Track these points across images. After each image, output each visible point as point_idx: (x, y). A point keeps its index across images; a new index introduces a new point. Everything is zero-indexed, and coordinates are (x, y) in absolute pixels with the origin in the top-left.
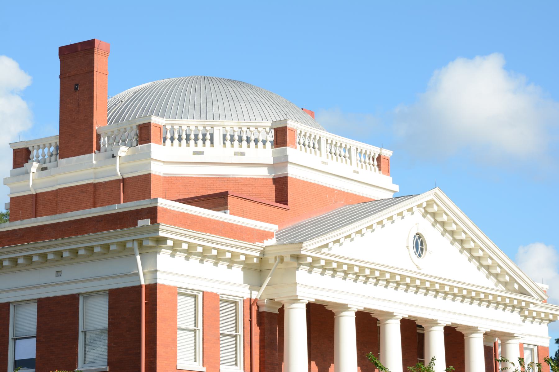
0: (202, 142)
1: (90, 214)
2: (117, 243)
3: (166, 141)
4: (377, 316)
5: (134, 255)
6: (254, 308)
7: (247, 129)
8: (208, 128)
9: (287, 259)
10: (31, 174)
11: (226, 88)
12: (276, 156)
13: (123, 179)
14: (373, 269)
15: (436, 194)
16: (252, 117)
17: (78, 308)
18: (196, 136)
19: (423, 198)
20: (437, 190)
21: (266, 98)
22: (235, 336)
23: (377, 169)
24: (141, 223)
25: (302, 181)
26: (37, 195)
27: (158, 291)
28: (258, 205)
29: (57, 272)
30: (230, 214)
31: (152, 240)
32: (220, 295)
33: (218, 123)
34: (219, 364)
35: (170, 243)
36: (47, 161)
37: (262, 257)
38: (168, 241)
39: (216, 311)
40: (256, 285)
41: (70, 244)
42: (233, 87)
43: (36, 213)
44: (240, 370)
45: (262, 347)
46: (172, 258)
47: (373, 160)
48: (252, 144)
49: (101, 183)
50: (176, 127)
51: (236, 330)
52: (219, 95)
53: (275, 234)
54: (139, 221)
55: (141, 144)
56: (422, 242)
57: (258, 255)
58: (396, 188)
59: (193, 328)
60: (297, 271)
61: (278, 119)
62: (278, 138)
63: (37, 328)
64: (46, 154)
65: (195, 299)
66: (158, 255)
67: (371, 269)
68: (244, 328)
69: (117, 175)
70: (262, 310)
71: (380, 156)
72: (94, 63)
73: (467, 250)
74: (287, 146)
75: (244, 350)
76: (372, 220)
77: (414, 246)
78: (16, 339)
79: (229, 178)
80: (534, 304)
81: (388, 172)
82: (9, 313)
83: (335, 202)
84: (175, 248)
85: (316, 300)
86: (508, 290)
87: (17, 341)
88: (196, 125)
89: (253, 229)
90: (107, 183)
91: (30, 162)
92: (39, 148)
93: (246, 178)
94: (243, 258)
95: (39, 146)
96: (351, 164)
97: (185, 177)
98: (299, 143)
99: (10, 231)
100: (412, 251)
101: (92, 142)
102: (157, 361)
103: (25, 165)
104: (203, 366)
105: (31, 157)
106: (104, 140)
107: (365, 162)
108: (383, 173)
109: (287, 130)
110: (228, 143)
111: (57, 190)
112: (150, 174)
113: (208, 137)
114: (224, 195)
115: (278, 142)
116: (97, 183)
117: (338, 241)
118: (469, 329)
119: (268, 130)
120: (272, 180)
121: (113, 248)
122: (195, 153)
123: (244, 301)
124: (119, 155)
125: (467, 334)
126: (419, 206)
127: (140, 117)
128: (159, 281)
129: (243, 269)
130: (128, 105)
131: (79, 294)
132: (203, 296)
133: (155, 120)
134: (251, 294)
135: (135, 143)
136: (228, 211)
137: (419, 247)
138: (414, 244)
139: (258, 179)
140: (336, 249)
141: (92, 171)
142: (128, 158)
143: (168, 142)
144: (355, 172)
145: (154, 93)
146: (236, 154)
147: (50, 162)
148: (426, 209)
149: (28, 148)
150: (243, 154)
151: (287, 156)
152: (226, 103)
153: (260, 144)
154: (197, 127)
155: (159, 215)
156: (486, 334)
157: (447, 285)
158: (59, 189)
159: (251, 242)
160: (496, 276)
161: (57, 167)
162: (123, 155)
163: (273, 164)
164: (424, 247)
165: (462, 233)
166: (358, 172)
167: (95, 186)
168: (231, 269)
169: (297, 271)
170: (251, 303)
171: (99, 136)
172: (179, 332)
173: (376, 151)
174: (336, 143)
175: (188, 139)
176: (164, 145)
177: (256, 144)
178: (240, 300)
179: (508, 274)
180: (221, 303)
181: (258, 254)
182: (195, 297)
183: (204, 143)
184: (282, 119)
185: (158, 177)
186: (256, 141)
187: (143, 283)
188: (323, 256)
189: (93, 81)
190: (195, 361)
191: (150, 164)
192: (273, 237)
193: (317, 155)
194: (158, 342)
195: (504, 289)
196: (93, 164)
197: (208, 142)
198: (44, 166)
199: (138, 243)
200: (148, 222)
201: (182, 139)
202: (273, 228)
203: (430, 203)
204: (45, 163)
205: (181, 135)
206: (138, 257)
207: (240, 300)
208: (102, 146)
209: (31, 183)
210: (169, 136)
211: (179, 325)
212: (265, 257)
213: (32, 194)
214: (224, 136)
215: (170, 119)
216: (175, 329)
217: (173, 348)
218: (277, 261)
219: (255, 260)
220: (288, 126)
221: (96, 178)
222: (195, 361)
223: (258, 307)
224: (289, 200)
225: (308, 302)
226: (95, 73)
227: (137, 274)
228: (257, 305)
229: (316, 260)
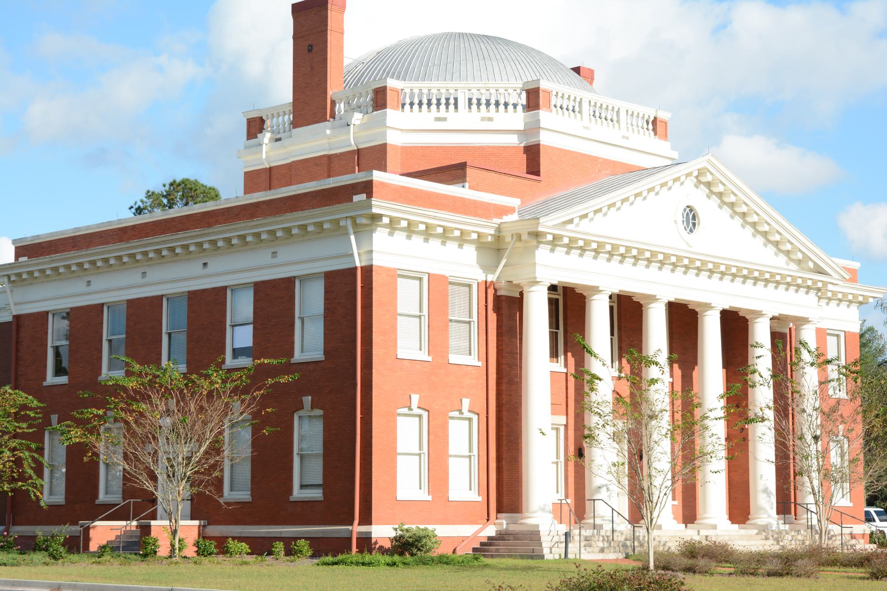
0: (445, 107)
2: (330, 221)
3: (405, 107)
4: (638, 299)
5: (347, 234)
6: (491, 292)
7: (504, 92)
8: (452, 91)
9: (525, 237)
10: (264, 145)
11: (477, 45)
13: (358, 149)
14: (629, 247)
15: (709, 161)
18: (439, 100)
19: (694, 166)
20: (709, 157)
21: (524, 55)
22: (469, 323)
23: (652, 133)
24: (356, 198)
25: (558, 149)
27: (374, 273)
28: (503, 176)
30: (470, 188)
31: (366, 217)
32: (450, 278)
33: (463, 85)
34: (448, 353)
35: (386, 220)
36: (282, 131)
37: (497, 234)
40: (488, 268)
41: (282, 222)
42: (486, 44)
43: (270, 186)
44: (474, 359)
47: (648, 123)
48: (502, 107)
49: (336, 154)
51: (470, 315)
52: (468, 54)
55: (377, 111)
56: (694, 217)
57: (492, 232)
58: (675, 155)
59: (418, 313)
60: (536, 251)
61: (530, 79)
62: (530, 101)
64: (274, 124)
65: (420, 282)
66: (374, 234)
67: (626, 247)
70: (499, 293)
71: (655, 118)
72: (327, 21)
73: (749, 224)
74: (539, 109)
75: (478, 338)
76: (629, 191)
77: (683, 221)
78: (235, 326)
79: (475, 147)
81: (665, 137)
83: (599, 171)
84: (393, 224)
85: (559, 282)
86: (803, 269)
87: (236, 328)
88: (477, 87)
89: (489, 204)
91: (264, 131)
92: (279, 116)
93: (494, 147)
95: (284, 112)
96: (619, 129)
97: (425, 147)
98: (555, 106)
99: (226, 208)
100: (681, 227)
101: (326, 109)
102: (373, 350)
103: (259, 135)
104: (429, 355)
106: (341, 107)
107: (643, 128)
108: (660, 138)
109: (540, 91)
110: (474, 107)
111: (290, 163)
113: (452, 101)
114: (462, 166)
115: (530, 105)
116: (331, 155)
117: (585, 216)
118: (753, 313)
119: (518, 91)
120: (523, 148)
121: (326, 226)
123: (478, 283)
124: (353, 123)
125: (751, 318)
126: (688, 175)
127: (374, 80)
129: (477, 248)
130: (369, 67)
131: (295, 277)
132: (845, 336)
133: (391, 83)
134: (486, 276)
135: (370, 109)
136: (467, 184)
138: (683, 218)
139: (508, 147)
140: (585, 226)
142: (363, 127)
143: (407, 107)
144: (623, 137)
145: (397, 53)
146: (483, 119)
147: (284, 132)
149: (262, 117)
150: (490, 119)
151: (539, 120)
153: (510, 107)
154: (439, 90)
156: (773, 319)
157: (722, 264)
158: (293, 162)
159: (487, 218)
160: (787, 253)
161: (291, 137)
162: (358, 123)
163: (524, 130)
164: (697, 222)
165: (743, 205)
166: (627, 138)
167: (330, 158)
169: (536, 251)
170: (487, 285)
171: (333, 103)
172: (399, 318)
173: (651, 113)
174: (601, 104)
176: (403, 111)
177: (506, 108)
178: (474, 282)
179: (800, 250)
180: (450, 286)
182: (420, 279)
183: (447, 108)
184: (535, 78)
185: (395, 147)
186: (506, 105)
187: (358, 264)
188: (567, 233)
190: (421, 350)
191: (386, 132)
192: (515, 212)
193: (484, 122)
196: (327, 135)
197: (452, 107)
198: (278, 136)
199: (352, 221)
200: (363, 197)
203: (701, 172)
204: (279, 133)
205: (431, 100)
206: (352, 237)
207: (474, 282)
208: (337, 113)
209: (264, 157)
210: (408, 101)
211: (399, 311)
212: (501, 234)
213: (266, 168)
214: (470, 100)
215: (412, 82)
216: (394, 315)
217: (392, 336)
218: (514, 240)
219: (490, 239)
220: (541, 87)
221: (330, 149)
222: (421, 350)
223: (496, 290)
224: (541, 171)
225: (549, 285)
226: (329, 32)
227: (352, 255)
228: (494, 288)
229: (556, 238)
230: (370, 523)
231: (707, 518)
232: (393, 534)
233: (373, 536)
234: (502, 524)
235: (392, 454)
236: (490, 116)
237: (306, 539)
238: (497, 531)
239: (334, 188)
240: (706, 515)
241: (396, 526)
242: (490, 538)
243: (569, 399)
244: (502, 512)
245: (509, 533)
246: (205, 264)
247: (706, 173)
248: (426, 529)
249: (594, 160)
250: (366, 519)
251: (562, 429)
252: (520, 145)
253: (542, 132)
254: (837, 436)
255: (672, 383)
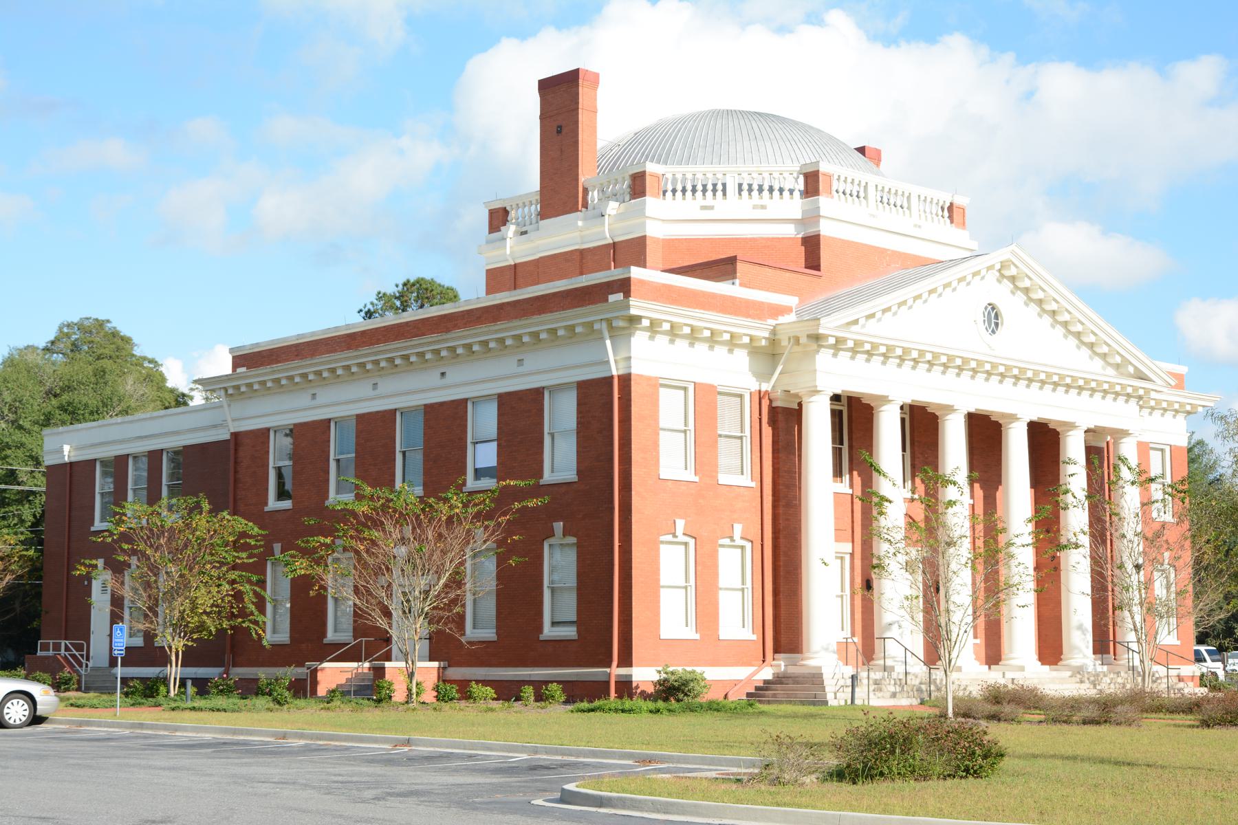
1: (553, 288)
2: (583, 324)
5: (602, 339)
6: (765, 403)
8: (720, 176)
9: (803, 340)
10: (508, 240)
11: (748, 123)
12: (807, 208)
15: (1013, 252)
16: (779, 160)
17: (543, 405)
18: (704, 186)
22: (741, 438)
24: (612, 298)
26: (515, 265)
28: (779, 272)
29: (519, 360)
30: (741, 285)
31: (623, 319)
34: (717, 472)
35: (646, 323)
37: (772, 337)
38: (643, 320)
39: (713, 407)
40: (763, 376)
45: (775, 451)
46: (651, 342)
47: (943, 209)
48: (776, 193)
49: (589, 248)
50: (679, 176)
53: (794, 310)
54: (610, 296)
56: (996, 316)
63: (498, 429)
68: (751, 427)
69: (606, 238)
70: (774, 404)
71: (951, 204)
74: (818, 195)
78: (477, 443)
79: (746, 239)
80: (1156, 391)
82: (466, 412)
84: (654, 327)
86: (1122, 374)
87: (478, 446)
90: (596, 249)
92: (525, 206)
94: (746, 340)
95: (531, 202)
96: (911, 216)
98: (837, 191)
101: (578, 197)
105: (509, 218)
106: (594, 196)
110: (745, 193)
112: (644, 237)
113: (720, 187)
114: (732, 261)
116: (584, 249)
117: (872, 316)
122: (703, 208)
123: (751, 393)
126: (990, 268)
127: (632, 164)
128: (634, 371)
129: (750, 354)
130: (625, 149)
133: (651, 168)
134: (760, 385)
135: (627, 198)
136: (737, 281)
137: (993, 321)
141: (577, 234)
142: (620, 217)
143: (669, 194)
146: (755, 207)
147: (531, 224)
148: (1003, 272)
150: (763, 207)
152: (746, 143)
153: (786, 193)
155: (632, 288)
158: (541, 258)
160: (1104, 356)
164: (999, 321)
167: (582, 252)
168: (732, 353)
170: (761, 396)
171: (586, 191)
172: (661, 433)
173: (947, 199)
175: (694, 190)
177: (781, 194)
179: (1118, 353)
180: (719, 397)
181: (766, 334)
183: (714, 195)
184: (814, 160)
185: (656, 240)
186: (781, 190)
187: (615, 373)
188: (852, 335)
189: (578, 121)
194: (633, 446)
195: (1115, 373)
197: (719, 194)
198: (524, 229)
200: (620, 296)
201: (707, 191)
202: (791, 301)
203: (1004, 265)
206: (608, 342)
209: (508, 252)
210: (670, 188)
211: (662, 424)
214: (740, 185)
216: (656, 431)
222: (686, 469)
223: (771, 401)
226: (580, 111)
227: (608, 362)
229: (839, 341)
230: (630, 665)
231: (1013, 658)
232: (656, 677)
233: (634, 679)
234: (780, 666)
235: (655, 586)
236: (763, 204)
237: (559, 682)
238: (774, 674)
239: (587, 287)
240: (1013, 655)
241: (660, 669)
242: (766, 682)
243: (855, 524)
244: (780, 653)
245: (788, 675)
246: (443, 374)
247: (1009, 266)
248: (694, 672)
249: (882, 252)
250: (626, 660)
251: (848, 558)
252: (798, 236)
253: (822, 221)
254: (1163, 565)
255: (973, 505)
